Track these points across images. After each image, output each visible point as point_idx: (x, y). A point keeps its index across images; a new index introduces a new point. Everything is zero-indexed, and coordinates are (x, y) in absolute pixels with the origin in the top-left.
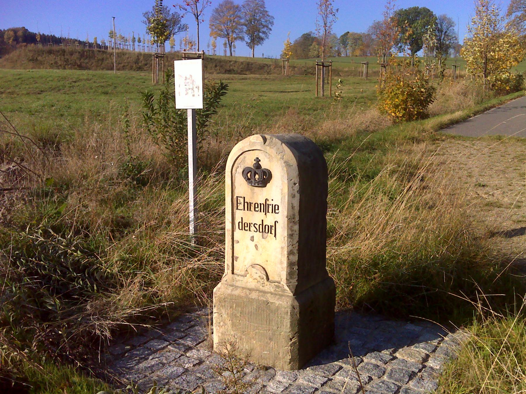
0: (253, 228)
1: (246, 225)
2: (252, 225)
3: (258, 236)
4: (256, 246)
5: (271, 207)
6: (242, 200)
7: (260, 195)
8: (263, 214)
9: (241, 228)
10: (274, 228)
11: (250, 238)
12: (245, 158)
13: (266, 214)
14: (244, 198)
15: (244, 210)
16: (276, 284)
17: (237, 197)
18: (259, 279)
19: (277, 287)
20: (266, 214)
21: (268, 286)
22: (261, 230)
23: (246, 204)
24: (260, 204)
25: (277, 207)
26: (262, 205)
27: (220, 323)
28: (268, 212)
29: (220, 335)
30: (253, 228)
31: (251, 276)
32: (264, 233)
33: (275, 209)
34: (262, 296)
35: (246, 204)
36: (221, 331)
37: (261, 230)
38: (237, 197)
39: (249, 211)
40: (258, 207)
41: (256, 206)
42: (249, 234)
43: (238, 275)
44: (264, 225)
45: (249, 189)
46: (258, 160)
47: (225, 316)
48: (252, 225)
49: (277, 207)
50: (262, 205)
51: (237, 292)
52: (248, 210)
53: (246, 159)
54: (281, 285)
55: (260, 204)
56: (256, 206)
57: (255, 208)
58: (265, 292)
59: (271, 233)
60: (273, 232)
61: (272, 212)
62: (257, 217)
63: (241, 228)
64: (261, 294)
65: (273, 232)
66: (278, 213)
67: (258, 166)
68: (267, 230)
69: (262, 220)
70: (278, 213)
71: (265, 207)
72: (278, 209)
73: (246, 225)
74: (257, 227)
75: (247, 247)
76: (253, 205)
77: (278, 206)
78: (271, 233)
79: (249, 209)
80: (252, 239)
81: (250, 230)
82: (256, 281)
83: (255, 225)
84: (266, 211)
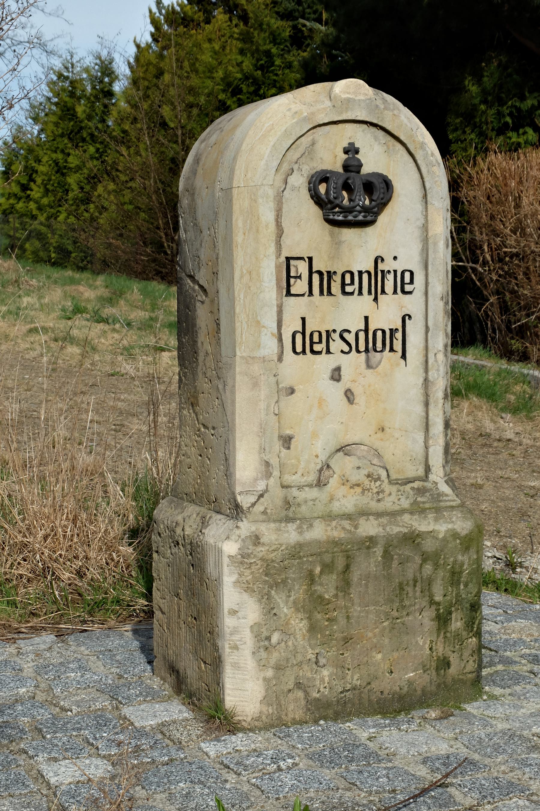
0: (337, 345)
1: (316, 338)
2: (336, 336)
3: (351, 364)
4: (349, 395)
5: (390, 277)
6: (302, 268)
7: (359, 249)
8: (367, 299)
9: (299, 349)
10: (399, 335)
11: (328, 374)
12: (313, 144)
13: (376, 299)
14: (310, 259)
15: (311, 293)
16: (416, 484)
17: (288, 259)
18: (367, 482)
19: (421, 491)
20: (376, 299)
21: (393, 498)
22: (362, 347)
23: (316, 278)
24: (360, 273)
25: (407, 275)
26: (365, 277)
27: (268, 638)
28: (383, 292)
29: (270, 673)
30: (337, 345)
31: (345, 481)
32: (372, 354)
33: (403, 284)
34: (390, 523)
35: (316, 278)
36: (273, 661)
37: (362, 347)
38: (288, 259)
39: (326, 299)
40: (352, 283)
41: (348, 280)
42: (324, 363)
43: (300, 488)
44: (372, 327)
45: (327, 232)
46: (351, 150)
47: (285, 610)
48: (336, 336)
49: (407, 275)
50: (365, 277)
51: (319, 532)
52: (321, 293)
53: (318, 146)
54: (428, 485)
55: (360, 273)
56: (348, 280)
57: (343, 285)
58: (394, 514)
59: (392, 350)
60: (398, 345)
61: (395, 292)
62: (350, 312)
63: (299, 349)
64: (384, 520)
65: (398, 345)
66: (410, 293)
67: (352, 166)
68: (375, 342)
69: (366, 318)
70: (410, 293)
71: (375, 281)
72: (412, 282)
73: (316, 338)
74: (350, 338)
75: (321, 402)
76: (338, 278)
77: (412, 273)
78: (392, 350)
79: (326, 291)
80: (336, 375)
81: (328, 352)
82: (359, 490)
83: (346, 335)
84: (377, 292)
